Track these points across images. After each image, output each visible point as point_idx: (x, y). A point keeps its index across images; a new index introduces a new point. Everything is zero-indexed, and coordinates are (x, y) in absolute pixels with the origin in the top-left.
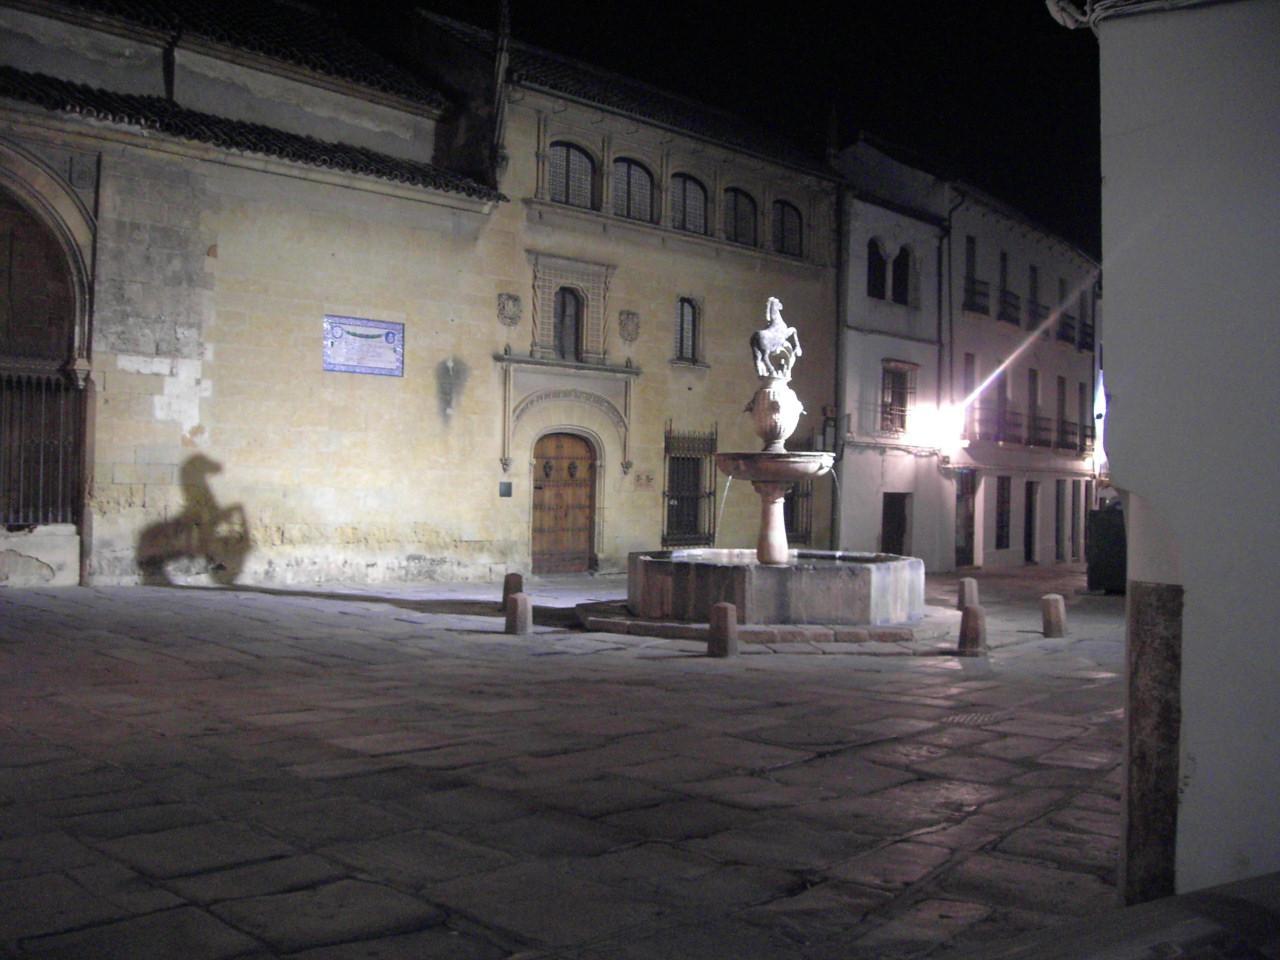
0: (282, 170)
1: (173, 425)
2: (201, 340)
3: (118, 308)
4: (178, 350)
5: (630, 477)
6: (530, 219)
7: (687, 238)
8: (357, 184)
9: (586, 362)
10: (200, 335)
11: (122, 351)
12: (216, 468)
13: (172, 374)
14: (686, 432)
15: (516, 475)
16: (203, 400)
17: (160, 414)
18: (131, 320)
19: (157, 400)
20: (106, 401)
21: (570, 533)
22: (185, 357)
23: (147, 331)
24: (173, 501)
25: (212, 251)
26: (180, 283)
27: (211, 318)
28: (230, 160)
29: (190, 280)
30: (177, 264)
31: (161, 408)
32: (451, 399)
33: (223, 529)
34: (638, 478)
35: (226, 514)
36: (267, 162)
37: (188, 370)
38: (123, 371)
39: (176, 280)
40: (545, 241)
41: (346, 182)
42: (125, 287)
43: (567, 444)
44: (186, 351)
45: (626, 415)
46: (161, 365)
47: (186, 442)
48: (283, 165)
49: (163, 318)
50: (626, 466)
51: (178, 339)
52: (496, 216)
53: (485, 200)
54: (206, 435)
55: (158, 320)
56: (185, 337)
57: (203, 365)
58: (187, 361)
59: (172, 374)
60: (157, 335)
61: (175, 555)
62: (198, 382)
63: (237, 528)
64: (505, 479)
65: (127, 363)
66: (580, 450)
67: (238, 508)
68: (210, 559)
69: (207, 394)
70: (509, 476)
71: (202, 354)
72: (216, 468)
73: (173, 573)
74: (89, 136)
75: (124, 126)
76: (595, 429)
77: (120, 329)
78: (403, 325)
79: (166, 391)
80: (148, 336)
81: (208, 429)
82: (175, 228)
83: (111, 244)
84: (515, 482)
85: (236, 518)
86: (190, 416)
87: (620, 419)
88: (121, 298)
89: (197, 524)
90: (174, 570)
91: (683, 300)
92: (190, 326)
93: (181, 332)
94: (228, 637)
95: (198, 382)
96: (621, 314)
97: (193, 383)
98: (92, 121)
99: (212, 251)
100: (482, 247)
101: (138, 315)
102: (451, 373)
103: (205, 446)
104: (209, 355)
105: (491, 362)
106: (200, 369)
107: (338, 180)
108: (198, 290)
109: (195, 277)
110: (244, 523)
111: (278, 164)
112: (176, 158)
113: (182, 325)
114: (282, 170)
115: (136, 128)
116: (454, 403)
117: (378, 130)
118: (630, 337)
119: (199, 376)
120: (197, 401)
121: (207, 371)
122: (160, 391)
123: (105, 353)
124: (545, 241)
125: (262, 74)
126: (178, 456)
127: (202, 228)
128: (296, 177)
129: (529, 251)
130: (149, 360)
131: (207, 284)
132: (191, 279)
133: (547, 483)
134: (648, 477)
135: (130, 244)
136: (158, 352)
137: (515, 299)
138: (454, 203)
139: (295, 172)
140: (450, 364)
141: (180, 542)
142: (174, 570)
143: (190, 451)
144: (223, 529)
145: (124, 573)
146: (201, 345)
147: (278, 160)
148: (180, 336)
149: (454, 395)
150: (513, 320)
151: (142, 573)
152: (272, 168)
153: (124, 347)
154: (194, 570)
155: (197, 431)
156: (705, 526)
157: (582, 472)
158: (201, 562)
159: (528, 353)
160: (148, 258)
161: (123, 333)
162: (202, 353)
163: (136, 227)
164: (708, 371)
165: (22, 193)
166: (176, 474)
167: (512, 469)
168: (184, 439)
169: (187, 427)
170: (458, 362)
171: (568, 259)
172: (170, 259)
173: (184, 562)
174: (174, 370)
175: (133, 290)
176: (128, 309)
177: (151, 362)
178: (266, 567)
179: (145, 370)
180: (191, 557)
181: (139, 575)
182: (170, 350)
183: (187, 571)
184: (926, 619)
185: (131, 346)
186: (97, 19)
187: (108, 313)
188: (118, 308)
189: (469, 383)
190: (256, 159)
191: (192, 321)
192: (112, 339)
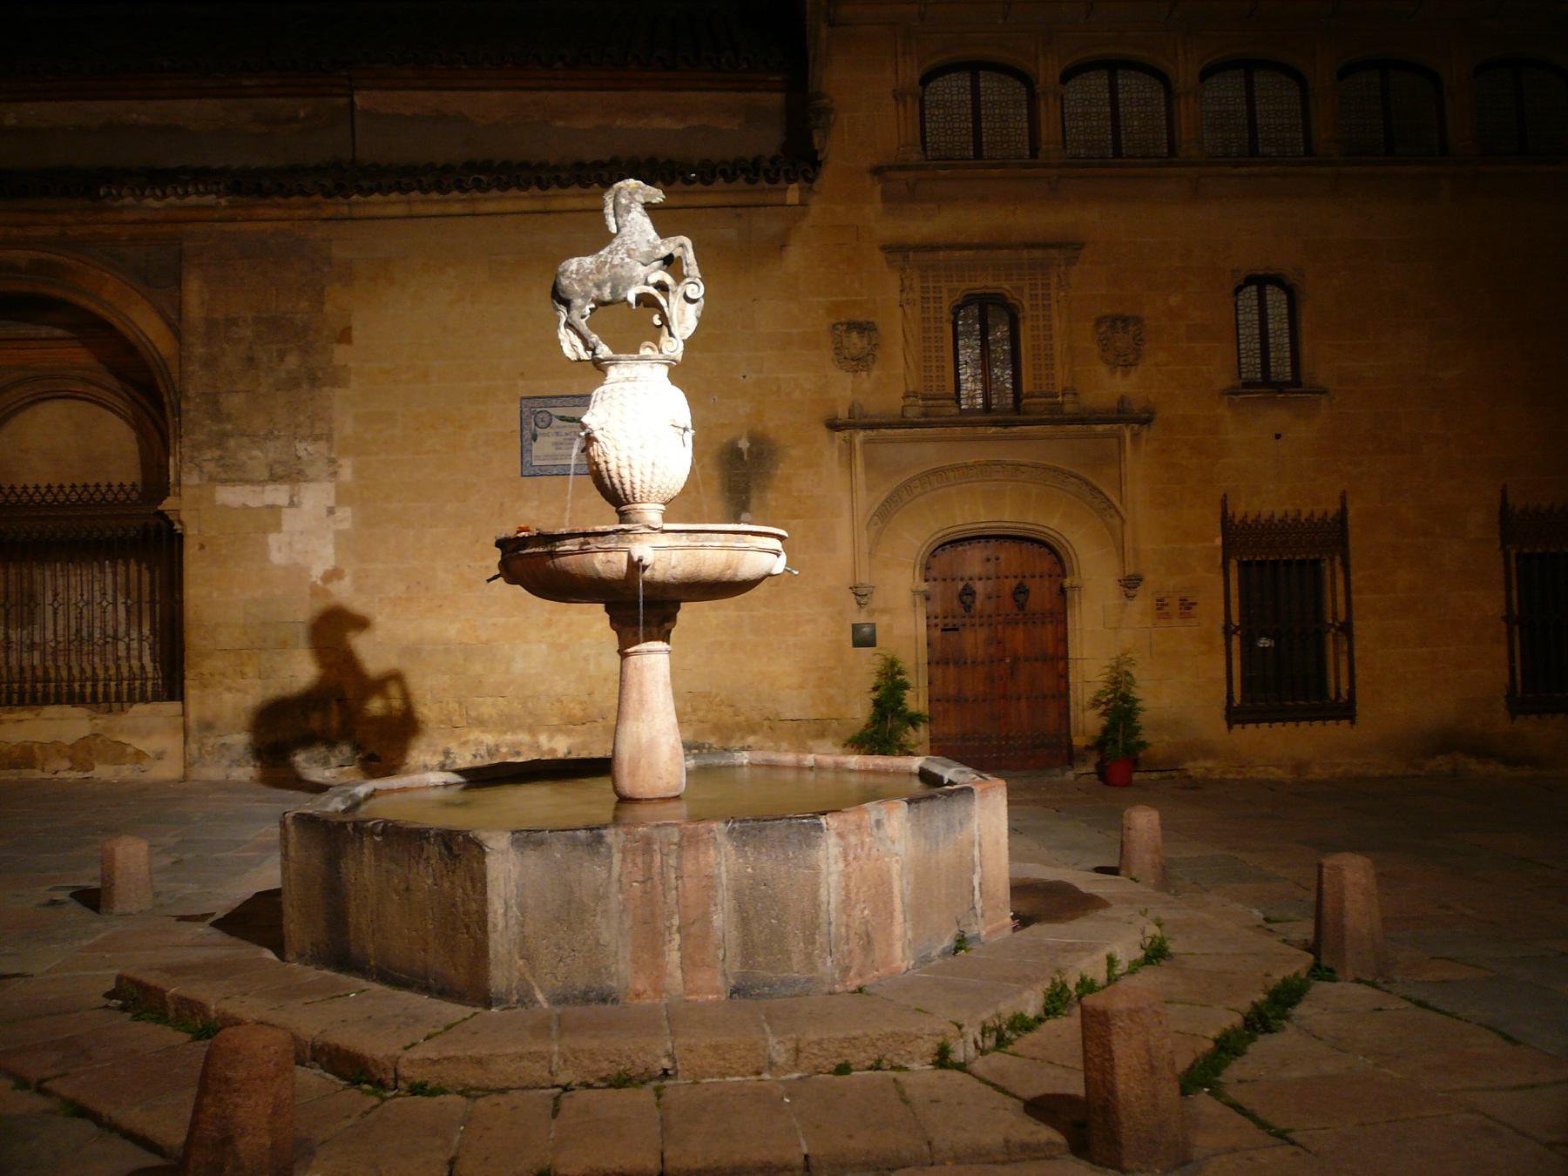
0: (435, 209)
1: (297, 572)
2: (333, 456)
3: (214, 428)
4: (300, 472)
5: (1141, 604)
6: (887, 198)
7: (1244, 170)
8: (556, 204)
9: (1026, 413)
10: (330, 449)
11: (224, 482)
12: (362, 623)
13: (292, 504)
14: (1278, 516)
15: (884, 611)
16: (338, 533)
17: (277, 557)
18: (232, 443)
19: (273, 539)
20: (202, 547)
21: (1023, 703)
22: (312, 481)
23: (256, 453)
24: (302, 671)
25: (345, 336)
26: (298, 385)
27: (346, 425)
28: (357, 212)
29: (314, 381)
30: (292, 361)
31: (278, 550)
32: (748, 498)
33: (376, 706)
34: (1161, 604)
35: (379, 685)
36: (409, 202)
37: (316, 496)
38: (225, 507)
39: (293, 383)
40: (921, 226)
41: (538, 205)
42: (221, 400)
43: (1009, 555)
44: (311, 471)
45: (1121, 502)
46: (277, 495)
47: (315, 591)
48: (432, 201)
49: (276, 433)
50: (1131, 583)
51: (299, 458)
52: (816, 207)
53: (782, 183)
54: (347, 581)
55: (270, 436)
56: (309, 454)
57: (337, 488)
58: (312, 485)
59: (292, 504)
60: (271, 455)
61: (308, 740)
62: (331, 511)
63: (397, 703)
64: (861, 618)
65: (229, 496)
66: (1044, 564)
67: (396, 677)
68: (358, 748)
69: (346, 525)
70: (871, 613)
71: (334, 474)
72: (362, 623)
73: (303, 764)
74: (133, 223)
75: (193, 200)
76: (1031, 520)
77: (217, 453)
78: (523, 398)
79: (285, 527)
80: (257, 458)
81: (347, 571)
82: (288, 316)
83: (199, 350)
84: (881, 621)
85: (394, 690)
86: (321, 557)
87: (1106, 508)
88: (217, 414)
89: (338, 700)
90: (306, 761)
91: (1261, 281)
92: (317, 439)
93: (302, 448)
94: (637, 837)
95: (331, 511)
96: (1098, 322)
97: (324, 512)
98: (151, 202)
99: (345, 336)
100: (795, 257)
101: (243, 434)
102: (746, 457)
103: (344, 593)
104: (346, 473)
105: (823, 432)
106: (333, 493)
107: (526, 205)
108: (326, 390)
109: (320, 374)
110: (406, 696)
111: (423, 202)
112: (281, 225)
113: (304, 438)
114: (435, 209)
115: (210, 199)
116: (754, 502)
117: (681, 126)
118: (1124, 361)
119: (331, 503)
120: (331, 536)
121: (343, 497)
122: (277, 527)
123: (198, 486)
124: (921, 226)
125: (483, 94)
126: (304, 612)
127: (328, 308)
128: (459, 215)
129: (887, 249)
130: (258, 489)
131: (337, 378)
132: (318, 378)
133: (967, 620)
134: (1183, 600)
135: (226, 346)
136: (274, 478)
137: (864, 328)
138: (733, 199)
139: (456, 208)
140: (744, 444)
141: (315, 722)
142: (306, 761)
143: (320, 605)
144: (376, 706)
145: (236, 763)
146: (332, 461)
147: (423, 197)
148: (302, 453)
149: (754, 494)
150: (858, 363)
151: (258, 764)
152: (420, 209)
153: (223, 476)
154: (334, 761)
155: (334, 575)
156: (1335, 682)
157: (1040, 593)
158: (346, 750)
159: (900, 412)
160: (251, 360)
161: (221, 458)
162: (336, 473)
163: (231, 322)
164: (1324, 400)
165: (92, 306)
166: (303, 633)
167: (877, 601)
168: (313, 586)
169: (317, 572)
170: (758, 440)
171: (969, 247)
172: (282, 356)
173: (319, 751)
174: (295, 499)
175: (234, 402)
176: (229, 427)
177: (263, 492)
178: (442, 758)
179: (254, 502)
180: (331, 744)
181: (255, 766)
182: (290, 474)
183: (326, 763)
184: (407, 1055)
185: (235, 474)
186: (246, 83)
187: (200, 436)
188: (214, 428)
189: (782, 469)
190: (388, 203)
191: (317, 432)
192: (210, 467)
